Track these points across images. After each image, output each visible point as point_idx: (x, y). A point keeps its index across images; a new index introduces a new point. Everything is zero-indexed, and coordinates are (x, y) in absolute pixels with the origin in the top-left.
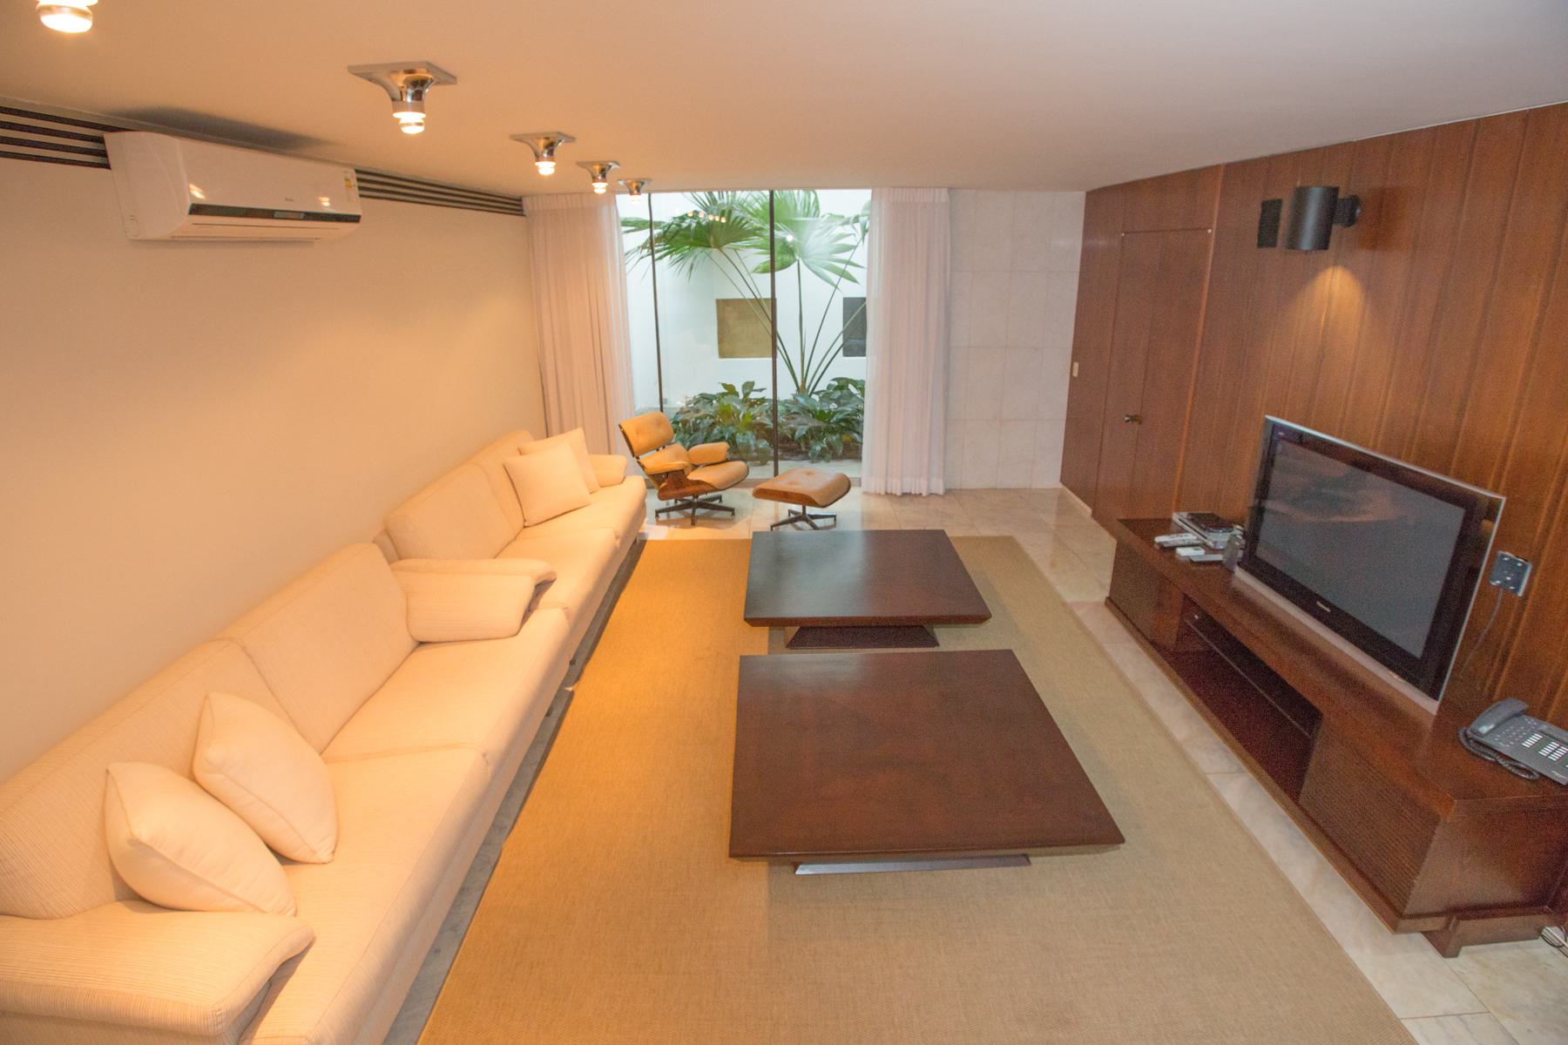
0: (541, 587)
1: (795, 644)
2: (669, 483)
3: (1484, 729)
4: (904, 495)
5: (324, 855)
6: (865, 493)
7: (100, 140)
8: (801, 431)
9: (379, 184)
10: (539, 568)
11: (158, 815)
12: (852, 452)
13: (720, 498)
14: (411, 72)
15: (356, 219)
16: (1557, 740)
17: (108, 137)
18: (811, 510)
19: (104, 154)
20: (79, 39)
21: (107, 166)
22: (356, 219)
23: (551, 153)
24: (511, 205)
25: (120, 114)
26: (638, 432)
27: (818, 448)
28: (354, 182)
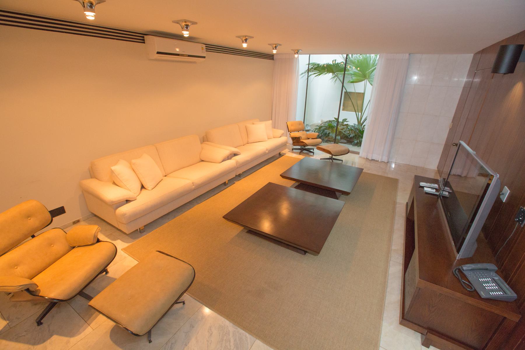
0: (235, 155)
1: (297, 187)
2: (296, 140)
3: (464, 268)
4: (372, 160)
5: (149, 189)
6: (360, 157)
7: (144, 37)
8: (352, 136)
9: (211, 48)
10: (235, 150)
11: (121, 169)
12: (359, 144)
13: (313, 149)
14: (185, 22)
15: (204, 57)
16: (497, 284)
17: (145, 36)
18: (334, 157)
19: (144, 40)
20: (92, 20)
21: (144, 43)
22: (204, 57)
23: (246, 41)
24: (271, 57)
25: (148, 32)
26: (292, 125)
27: (356, 142)
28: (205, 48)
